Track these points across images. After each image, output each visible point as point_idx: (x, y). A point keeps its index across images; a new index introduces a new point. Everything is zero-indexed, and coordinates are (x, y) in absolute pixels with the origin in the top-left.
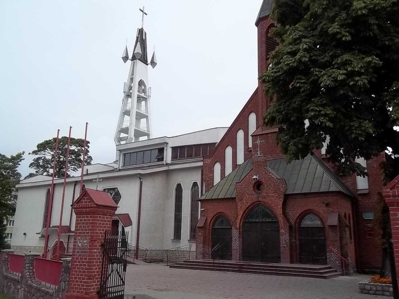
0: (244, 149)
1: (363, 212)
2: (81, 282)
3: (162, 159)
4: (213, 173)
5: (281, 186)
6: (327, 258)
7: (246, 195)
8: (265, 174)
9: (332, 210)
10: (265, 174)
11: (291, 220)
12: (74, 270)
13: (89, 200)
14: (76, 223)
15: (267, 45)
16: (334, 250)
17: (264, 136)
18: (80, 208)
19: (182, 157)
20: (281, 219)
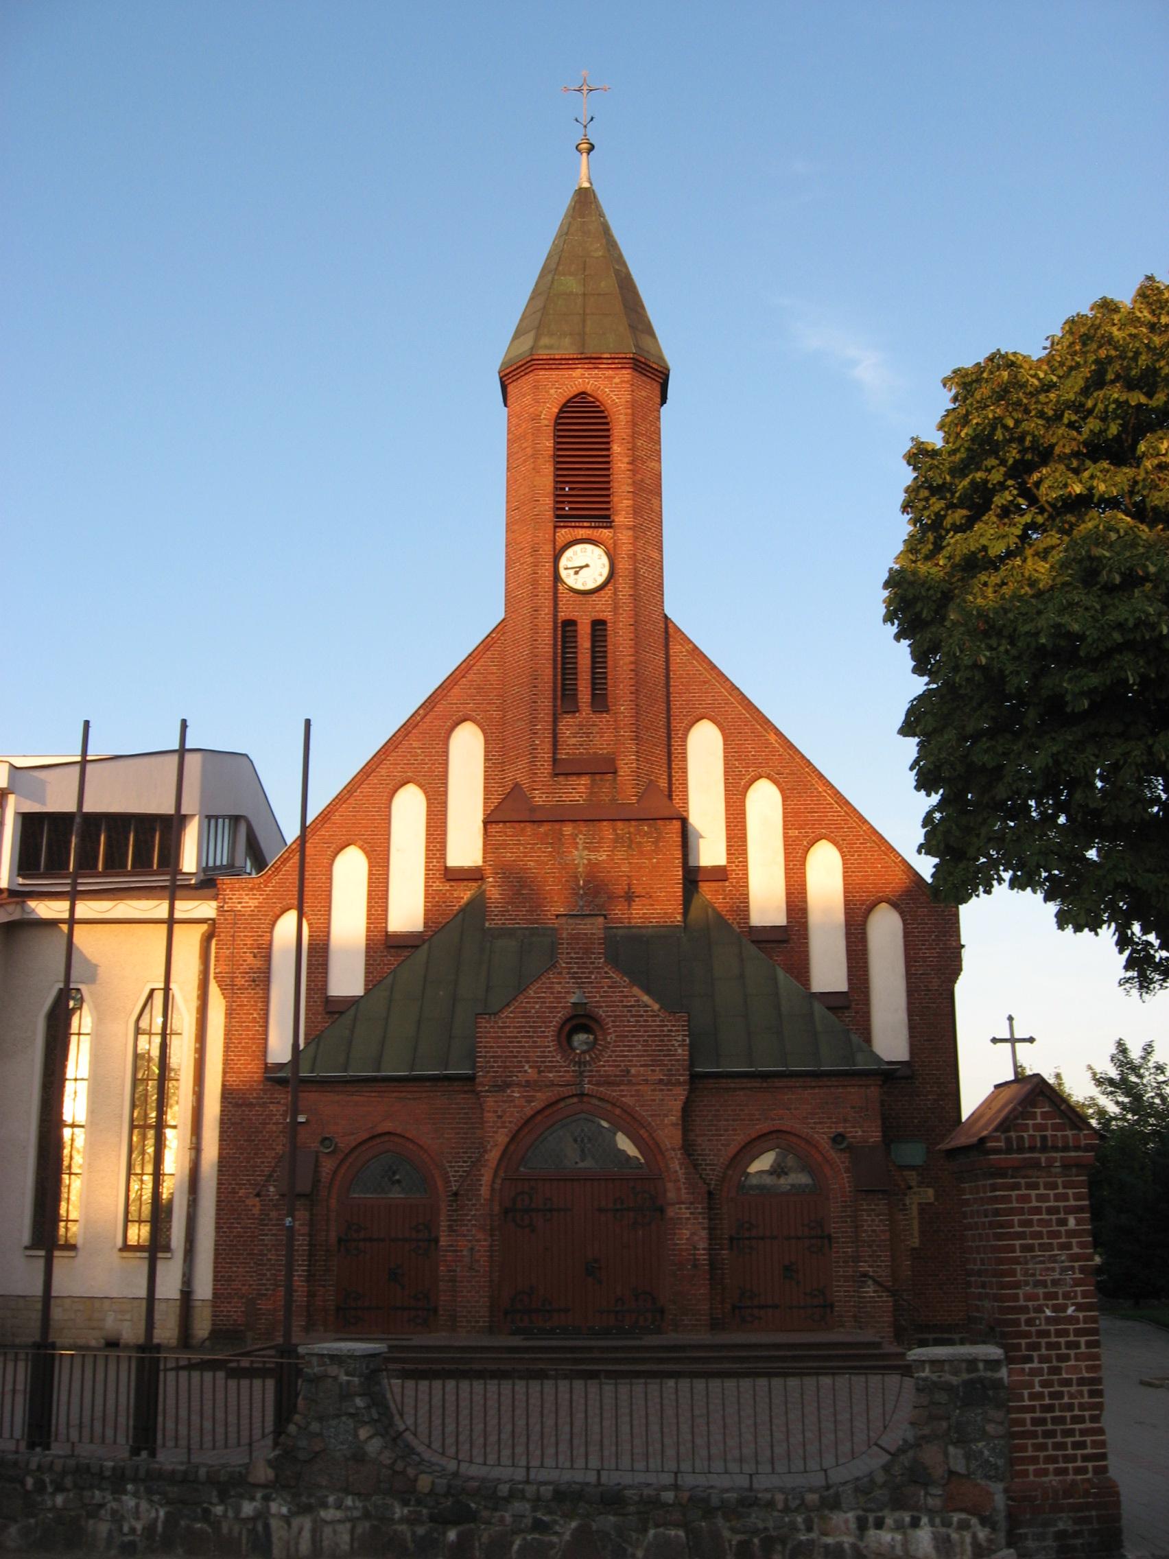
0: (427, 869)
2: (1070, 1433)
7: (527, 1068)
9: (860, 1133)
12: (1026, 1393)
17: (542, 830)
18: (1020, 1150)
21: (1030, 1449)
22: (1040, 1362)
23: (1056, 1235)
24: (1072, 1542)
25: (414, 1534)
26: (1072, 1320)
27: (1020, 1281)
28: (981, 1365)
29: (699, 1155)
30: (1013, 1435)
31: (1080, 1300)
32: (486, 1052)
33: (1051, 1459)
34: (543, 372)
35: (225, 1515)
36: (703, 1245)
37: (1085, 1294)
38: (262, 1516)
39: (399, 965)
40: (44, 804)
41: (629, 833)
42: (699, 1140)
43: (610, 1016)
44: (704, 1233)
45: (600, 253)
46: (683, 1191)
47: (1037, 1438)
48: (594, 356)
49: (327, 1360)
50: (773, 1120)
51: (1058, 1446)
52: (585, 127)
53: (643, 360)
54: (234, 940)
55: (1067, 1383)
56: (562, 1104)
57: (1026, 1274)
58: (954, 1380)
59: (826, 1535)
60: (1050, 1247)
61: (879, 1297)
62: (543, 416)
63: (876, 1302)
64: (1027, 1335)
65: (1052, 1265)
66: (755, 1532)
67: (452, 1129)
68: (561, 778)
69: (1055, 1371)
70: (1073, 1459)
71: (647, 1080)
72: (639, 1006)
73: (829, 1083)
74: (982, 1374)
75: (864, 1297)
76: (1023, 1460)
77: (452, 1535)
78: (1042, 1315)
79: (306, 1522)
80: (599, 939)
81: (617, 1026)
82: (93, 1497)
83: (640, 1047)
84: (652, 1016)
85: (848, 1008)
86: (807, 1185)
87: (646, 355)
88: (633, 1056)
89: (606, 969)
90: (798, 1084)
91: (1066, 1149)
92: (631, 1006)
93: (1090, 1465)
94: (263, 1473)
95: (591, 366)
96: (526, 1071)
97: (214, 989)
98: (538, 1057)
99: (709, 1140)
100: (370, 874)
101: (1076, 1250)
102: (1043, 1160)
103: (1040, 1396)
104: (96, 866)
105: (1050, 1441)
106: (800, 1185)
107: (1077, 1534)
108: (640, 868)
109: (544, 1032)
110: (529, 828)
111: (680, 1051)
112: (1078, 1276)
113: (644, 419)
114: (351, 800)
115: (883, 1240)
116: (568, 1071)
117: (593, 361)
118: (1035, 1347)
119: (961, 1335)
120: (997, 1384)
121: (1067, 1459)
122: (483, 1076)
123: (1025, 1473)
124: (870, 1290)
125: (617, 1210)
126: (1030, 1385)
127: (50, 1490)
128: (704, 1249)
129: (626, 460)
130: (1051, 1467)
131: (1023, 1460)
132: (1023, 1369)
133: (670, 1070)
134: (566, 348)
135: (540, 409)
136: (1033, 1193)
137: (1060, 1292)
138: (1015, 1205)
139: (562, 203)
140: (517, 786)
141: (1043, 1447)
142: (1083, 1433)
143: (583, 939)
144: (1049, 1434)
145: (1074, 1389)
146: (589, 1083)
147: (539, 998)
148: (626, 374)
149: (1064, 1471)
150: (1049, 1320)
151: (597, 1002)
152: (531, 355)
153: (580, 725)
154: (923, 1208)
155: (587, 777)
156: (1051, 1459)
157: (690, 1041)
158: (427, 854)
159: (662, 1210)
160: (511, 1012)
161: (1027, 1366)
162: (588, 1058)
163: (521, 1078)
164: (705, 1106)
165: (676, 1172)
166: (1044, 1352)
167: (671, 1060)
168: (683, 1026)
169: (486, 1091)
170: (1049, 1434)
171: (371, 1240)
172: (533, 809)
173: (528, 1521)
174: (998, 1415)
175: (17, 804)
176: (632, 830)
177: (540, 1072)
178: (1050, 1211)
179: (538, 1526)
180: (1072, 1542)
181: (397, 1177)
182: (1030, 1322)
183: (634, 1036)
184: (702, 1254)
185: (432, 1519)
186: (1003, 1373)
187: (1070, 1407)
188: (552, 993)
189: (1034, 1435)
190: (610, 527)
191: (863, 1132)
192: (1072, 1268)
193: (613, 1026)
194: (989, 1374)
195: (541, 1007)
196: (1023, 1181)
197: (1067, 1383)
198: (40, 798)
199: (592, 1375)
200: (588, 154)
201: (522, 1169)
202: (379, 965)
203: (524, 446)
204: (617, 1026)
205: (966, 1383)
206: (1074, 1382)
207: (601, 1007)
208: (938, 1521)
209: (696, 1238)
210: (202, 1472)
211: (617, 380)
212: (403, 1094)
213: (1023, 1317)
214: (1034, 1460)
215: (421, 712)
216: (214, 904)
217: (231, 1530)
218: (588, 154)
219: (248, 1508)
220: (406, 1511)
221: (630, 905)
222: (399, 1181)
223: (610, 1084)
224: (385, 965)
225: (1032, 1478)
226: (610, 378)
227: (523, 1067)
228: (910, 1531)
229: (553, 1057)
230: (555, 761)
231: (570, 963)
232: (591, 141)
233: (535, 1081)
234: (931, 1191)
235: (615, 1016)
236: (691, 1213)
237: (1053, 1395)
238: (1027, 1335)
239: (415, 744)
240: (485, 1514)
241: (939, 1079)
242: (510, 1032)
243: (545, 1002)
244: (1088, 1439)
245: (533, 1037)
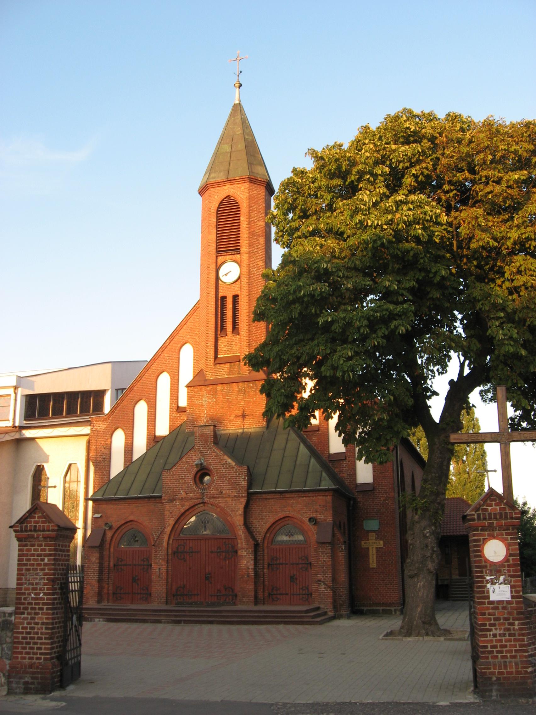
0: (171, 408)
1: (364, 520)
5: (242, 478)
7: (182, 492)
8: (215, 456)
10: (215, 456)
11: (257, 534)
12: (21, 626)
13: (44, 519)
14: (18, 554)
17: (209, 388)
18: (26, 531)
19: (43, 414)
20: (241, 532)
21: (20, 648)
22: (28, 614)
23: (39, 565)
24: (30, 686)
26: (42, 599)
27: (23, 583)
28: (7, 615)
29: (254, 528)
30: (15, 643)
31: (46, 591)
32: (166, 486)
33: (27, 653)
34: (212, 189)
36: (252, 567)
37: (48, 589)
40: (34, 390)
41: (244, 387)
42: (254, 521)
43: (215, 469)
44: (252, 562)
45: (240, 132)
46: (244, 544)
47: (23, 644)
48: (232, 179)
50: (286, 512)
51: (31, 648)
52: (238, 76)
53: (254, 178)
54: (97, 442)
55: (37, 624)
56: (197, 507)
57: (26, 580)
60: (36, 570)
61: (326, 590)
62: (212, 208)
63: (325, 593)
64: (24, 604)
65: (36, 577)
67: (156, 518)
68: (218, 366)
69: (33, 618)
70: (36, 654)
71: (229, 496)
72: (227, 464)
73: (310, 495)
74: (7, 618)
75: (320, 590)
76: (16, 653)
78: (30, 597)
80: (211, 436)
83: (227, 482)
84: (232, 468)
85: (345, 459)
86: (302, 541)
87: (255, 175)
88: (224, 486)
89: (214, 449)
90: (296, 496)
91: (44, 531)
93: (43, 657)
95: (232, 183)
96: (181, 494)
97: (91, 464)
99: (258, 521)
100: (148, 411)
101: (47, 571)
102: (35, 535)
103: (26, 628)
104: (62, 414)
105: (28, 646)
106: (299, 541)
107: (32, 683)
108: (249, 402)
109: (189, 476)
110: (203, 388)
111: (243, 483)
112: (46, 581)
113: (255, 203)
114: (141, 381)
115: (329, 565)
116: (198, 493)
117: (231, 181)
118: (26, 609)
120: (10, 622)
121: (34, 654)
122: (165, 496)
123: (17, 658)
124: (322, 587)
125: (218, 552)
126: (23, 623)
128: (252, 569)
129: (246, 223)
130: (27, 656)
131: (16, 653)
132: (20, 617)
133: (238, 491)
135: (211, 205)
136: (33, 548)
137: (38, 588)
138: (25, 552)
140: (202, 370)
141: (25, 648)
142: (41, 644)
143: (204, 436)
144: (28, 643)
145: (39, 626)
146: (206, 497)
147: (187, 462)
148: (247, 185)
149: (32, 658)
150: (33, 598)
151: (210, 463)
152: (207, 182)
153: (228, 342)
154: (378, 550)
155: (228, 364)
156: (27, 653)
157: (248, 478)
158: (170, 402)
159: (236, 552)
160: (176, 469)
161: (23, 616)
163: (179, 496)
164: (257, 506)
165: (241, 535)
166: (29, 611)
167: (239, 487)
168: (245, 472)
169: (166, 502)
170: (28, 643)
171: (126, 565)
172: (206, 380)
174: (9, 634)
175: (22, 392)
176: (245, 386)
177: (187, 494)
178: (38, 555)
180: (30, 686)
181: (137, 539)
182: (25, 599)
183: (224, 477)
184: (251, 572)
186: (13, 618)
187: (37, 633)
188: (192, 460)
189: (22, 643)
190: (239, 254)
191: (324, 516)
192: (44, 578)
193: (217, 473)
196: (29, 543)
197: (37, 624)
198: (32, 388)
199: (179, 622)
200: (239, 88)
201: (181, 535)
206: (40, 623)
207: (212, 465)
209: (249, 564)
211: (243, 188)
212: (137, 504)
213: (23, 597)
214: (21, 653)
215: (168, 341)
216: (89, 428)
218: (239, 88)
221: (244, 419)
222: (137, 541)
223: (214, 498)
225: (19, 660)
226: (240, 187)
229: (192, 487)
230: (216, 357)
231: (199, 447)
232: (241, 83)
233: (185, 498)
234: (382, 542)
235: (217, 469)
236: (247, 553)
237: (31, 628)
238: (24, 604)
239: (166, 355)
241: (386, 490)
243: (189, 464)
244: (43, 646)
245: (184, 479)
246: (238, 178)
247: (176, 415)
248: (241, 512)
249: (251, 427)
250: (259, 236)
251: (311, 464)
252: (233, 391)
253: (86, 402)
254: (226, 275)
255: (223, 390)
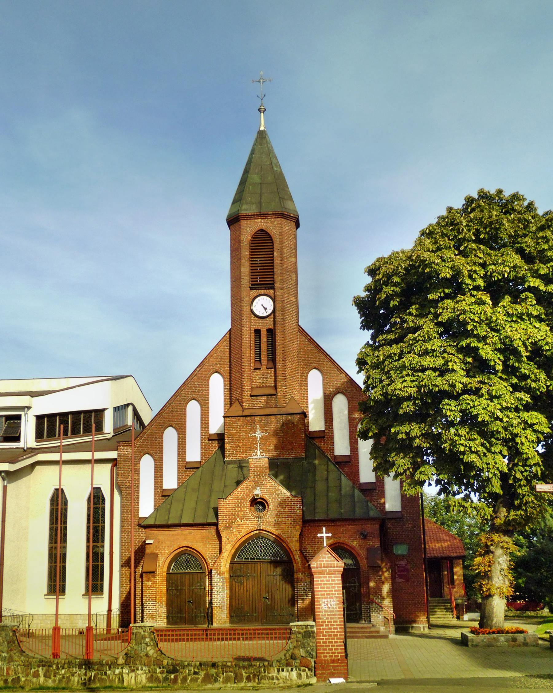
1: (394, 545)
3: (17, 439)
4: (138, 474)
6: (362, 613)
8: (270, 486)
10: (270, 486)
12: (321, 634)
15: (251, 255)
16: (377, 600)
17: (247, 419)
18: (321, 567)
19: (52, 435)
25: (162, 676)
35: (111, 674)
38: (121, 674)
39: (192, 475)
48: (265, 213)
49: (138, 628)
52: (262, 100)
58: (302, 631)
59: (270, 674)
66: (251, 673)
77: (172, 676)
79: (133, 674)
80: (266, 467)
81: (273, 502)
82: (73, 670)
85: (375, 489)
89: (269, 479)
92: (279, 494)
94: (121, 661)
96: (238, 521)
98: (242, 515)
111: (298, 511)
117: (263, 215)
119: (423, 625)
120: (313, 632)
126: (323, 632)
127: (60, 669)
134: (253, 209)
139: (254, 136)
142: (337, 646)
149: (332, 656)
151: (265, 492)
160: (232, 497)
162: (262, 515)
166: (327, 623)
173: (192, 672)
179: (195, 673)
185: (167, 672)
188: (248, 489)
194: (311, 629)
195: (243, 495)
202: (183, 475)
203: (237, 253)
204: (273, 502)
205: (305, 632)
208: (298, 669)
210: (104, 662)
211: (275, 223)
217: (112, 678)
219: (117, 671)
220: (160, 670)
224: (186, 475)
227: (237, 519)
228: (291, 672)
240: (181, 670)
242: (231, 505)
246: (271, 213)
247: (207, 442)
248: (297, 538)
249: (290, 457)
250: (291, 271)
251: (356, 495)
252: (271, 422)
253: (88, 422)
254: (265, 309)
255: (261, 421)
